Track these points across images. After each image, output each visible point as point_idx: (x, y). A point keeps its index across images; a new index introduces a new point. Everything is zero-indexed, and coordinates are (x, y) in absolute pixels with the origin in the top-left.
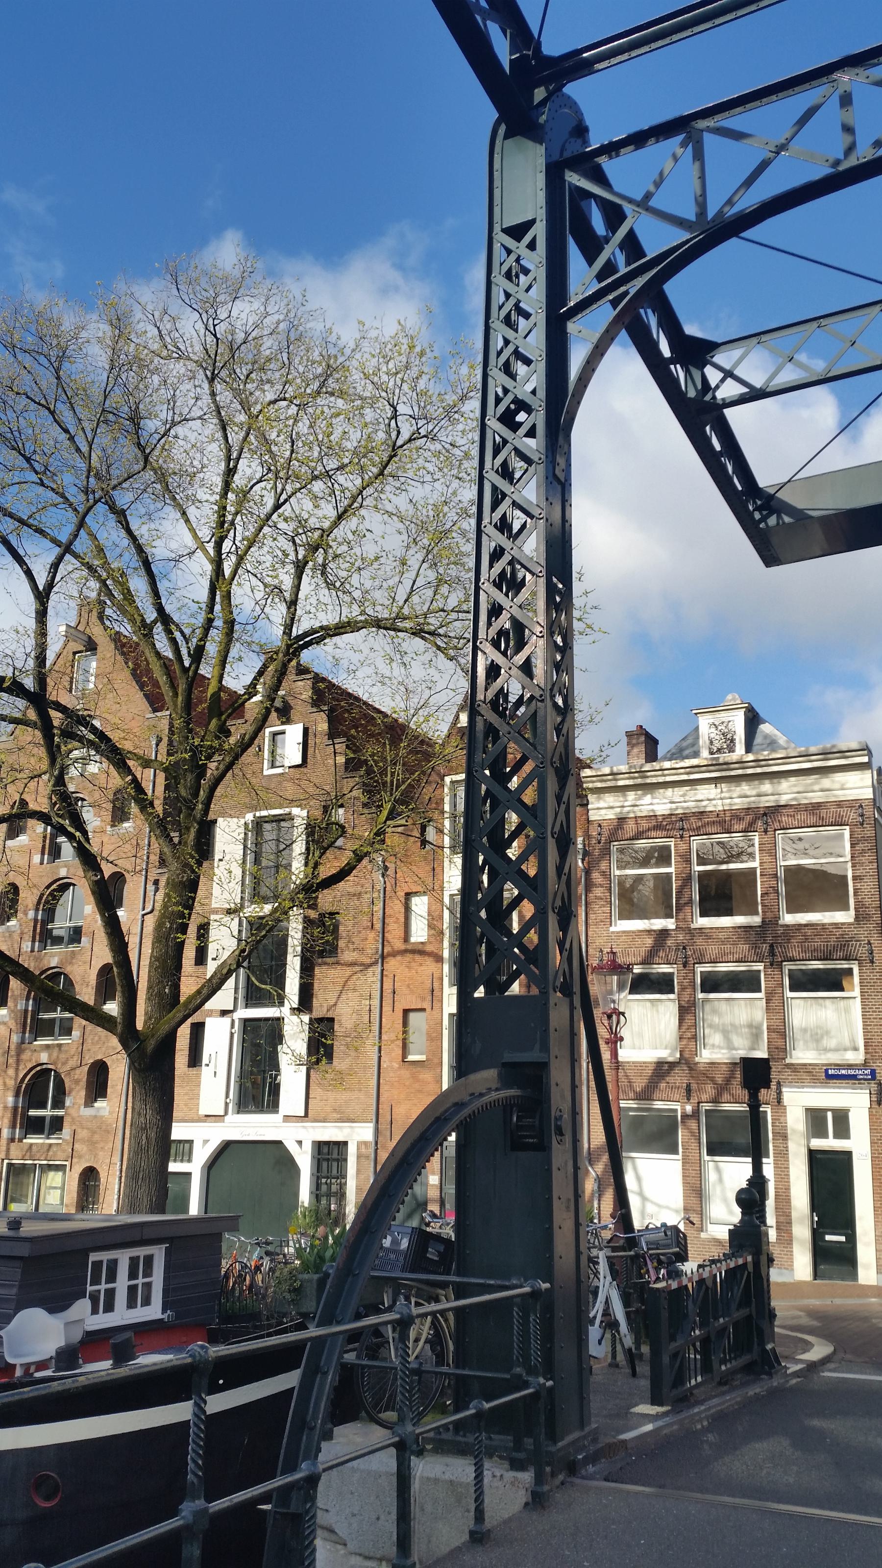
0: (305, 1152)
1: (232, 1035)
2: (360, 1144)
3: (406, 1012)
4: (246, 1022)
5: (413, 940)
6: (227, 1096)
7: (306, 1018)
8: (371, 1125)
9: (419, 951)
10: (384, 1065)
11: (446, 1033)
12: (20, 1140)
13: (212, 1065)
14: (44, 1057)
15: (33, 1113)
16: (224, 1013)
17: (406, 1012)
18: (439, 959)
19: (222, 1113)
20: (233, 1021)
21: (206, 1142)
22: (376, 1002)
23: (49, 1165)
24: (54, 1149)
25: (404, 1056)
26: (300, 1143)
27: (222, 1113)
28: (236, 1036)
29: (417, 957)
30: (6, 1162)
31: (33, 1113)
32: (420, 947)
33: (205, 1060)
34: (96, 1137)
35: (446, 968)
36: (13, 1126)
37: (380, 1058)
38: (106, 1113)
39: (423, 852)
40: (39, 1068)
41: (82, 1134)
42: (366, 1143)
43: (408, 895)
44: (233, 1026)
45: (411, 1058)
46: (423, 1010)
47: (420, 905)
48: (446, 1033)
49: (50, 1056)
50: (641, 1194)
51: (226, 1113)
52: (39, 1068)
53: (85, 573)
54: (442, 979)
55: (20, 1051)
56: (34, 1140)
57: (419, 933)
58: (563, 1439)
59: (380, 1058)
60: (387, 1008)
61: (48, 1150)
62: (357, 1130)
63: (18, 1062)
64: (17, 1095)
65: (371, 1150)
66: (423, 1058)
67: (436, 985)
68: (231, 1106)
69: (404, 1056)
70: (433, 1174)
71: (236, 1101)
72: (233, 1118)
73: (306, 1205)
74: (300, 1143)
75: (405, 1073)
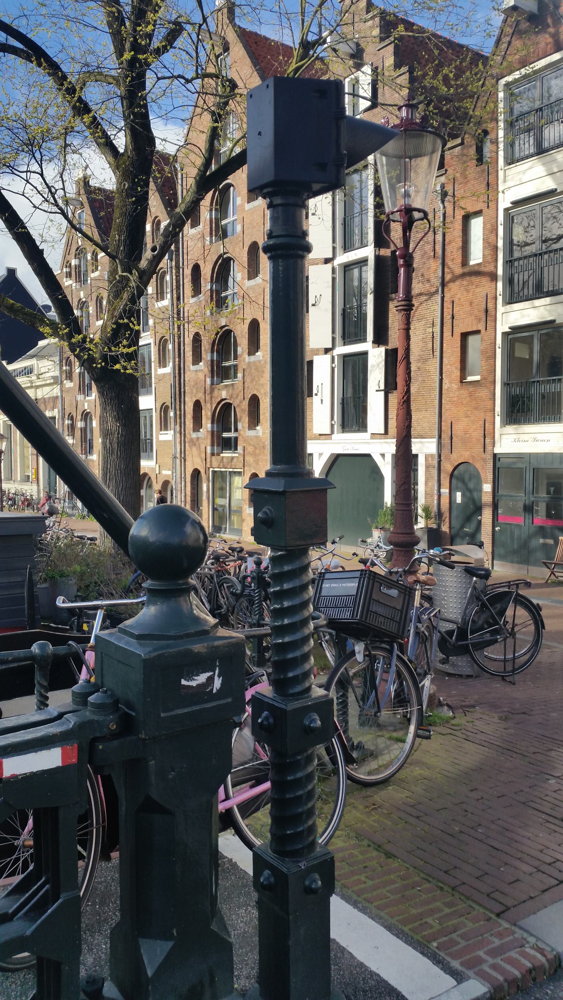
0: (388, 463)
1: (333, 369)
2: (427, 457)
3: (465, 336)
4: (345, 358)
5: (472, 263)
6: (332, 418)
7: (382, 349)
8: (435, 440)
9: (476, 273)
10: (445, 387)
11: (499, 352)
12: (218, 455)
13: (319, 394)
14: (224, 394)
15: (225, 435)
16: (327, 351)
17: (465, 336)
18: (493, 277)
19: (328, 432)
20: (333, 358)
21: (321, 455)
22: (437, 329)
23: (235, 472)
24: (235, 460)
25: (463, 376)
26: (383, 455)
27: (329, 432)
28: (336, 369)
29: (474, 279)
30: (211, 469)
31: (225, 435)
32: (476, 268)
33: (315, 391)
34: (257, 451)
35: (500, 285)
36: (212, 445)
37: (441, 380)
38: (260, 434)
39: (478, 169)
40: (223, 402)
41: (250, 449)
42: (432, 456)
43: (467, 218)
44: (333, 362)
45: (470, 379)
46: (478, 332)
47: (477, 226)
48: (499, 352)
49: (227, 392)
50: (241, 789)
51: (332, 432)
52: (223, 402)
53: (237, 11)
54: (496, 298)
55: (212, 390)
56: (227, 454)
57: (476, 256)
58: (496, 978)
59: (441, 380)
60: (447, 334)
61: (232, 461)
62: (426, 445)
63: (211, 398)
64: (213, 423)
65: (435, 462)
66: (478, 378)
67: (490, 305)
68: (336, 426)
69: (463, 376)
70: (487, 483)
71: (340, 423)
72: (338, 436)
73: (389, 505)
74: (383, 455)
75: (464, 393)
